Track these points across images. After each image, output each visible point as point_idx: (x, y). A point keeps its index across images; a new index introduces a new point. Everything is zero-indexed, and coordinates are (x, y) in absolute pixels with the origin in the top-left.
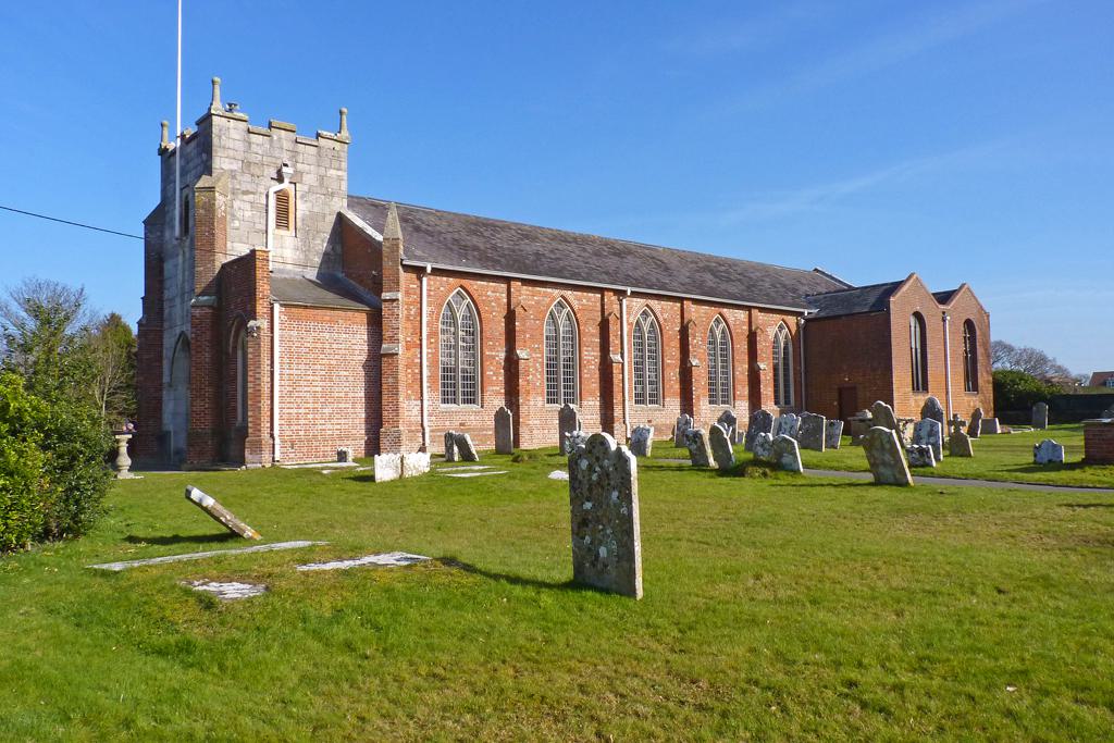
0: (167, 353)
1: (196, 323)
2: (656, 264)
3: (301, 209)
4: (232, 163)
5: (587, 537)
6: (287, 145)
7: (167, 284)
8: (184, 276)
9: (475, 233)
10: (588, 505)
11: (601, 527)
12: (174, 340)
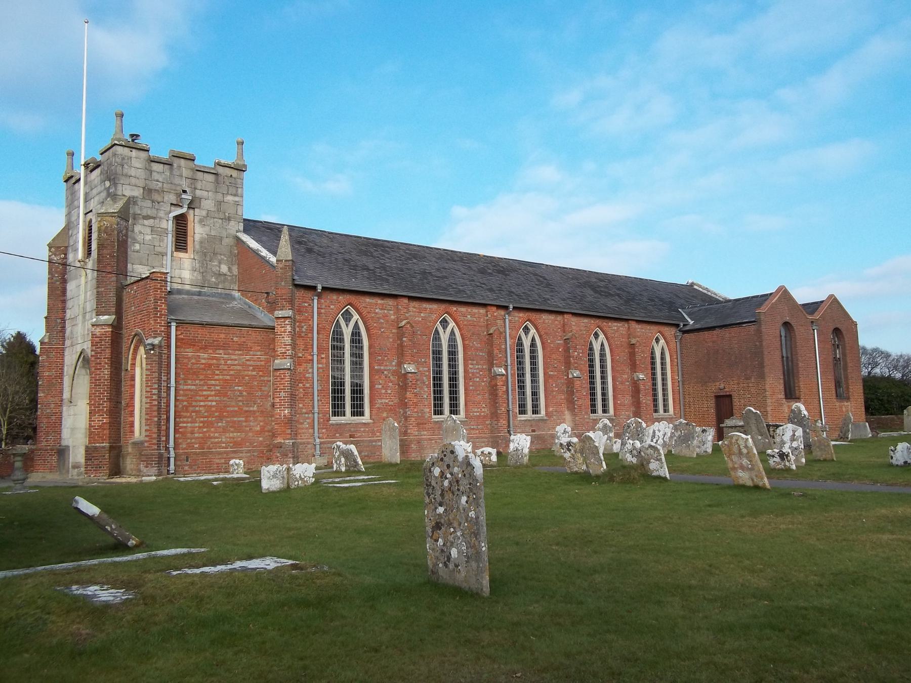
0: (68, 370)
1: (96, 342)
2: (538, 280)
3: (197, 231)
4: (132, 190)
5: (440, 540)
6: (186, 173)
7: (69, 304)
8: (85, 297)
9: (365, 253)
10: (441, 510)
11: (452, 530)
12: (76, 356)
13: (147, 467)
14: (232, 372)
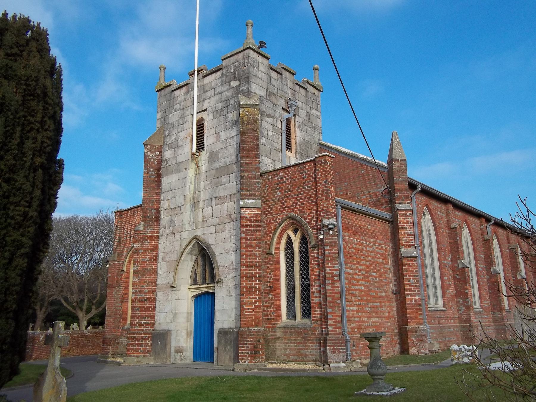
4: (260, 90)
13: (334, 352)
14: (370, 259)
